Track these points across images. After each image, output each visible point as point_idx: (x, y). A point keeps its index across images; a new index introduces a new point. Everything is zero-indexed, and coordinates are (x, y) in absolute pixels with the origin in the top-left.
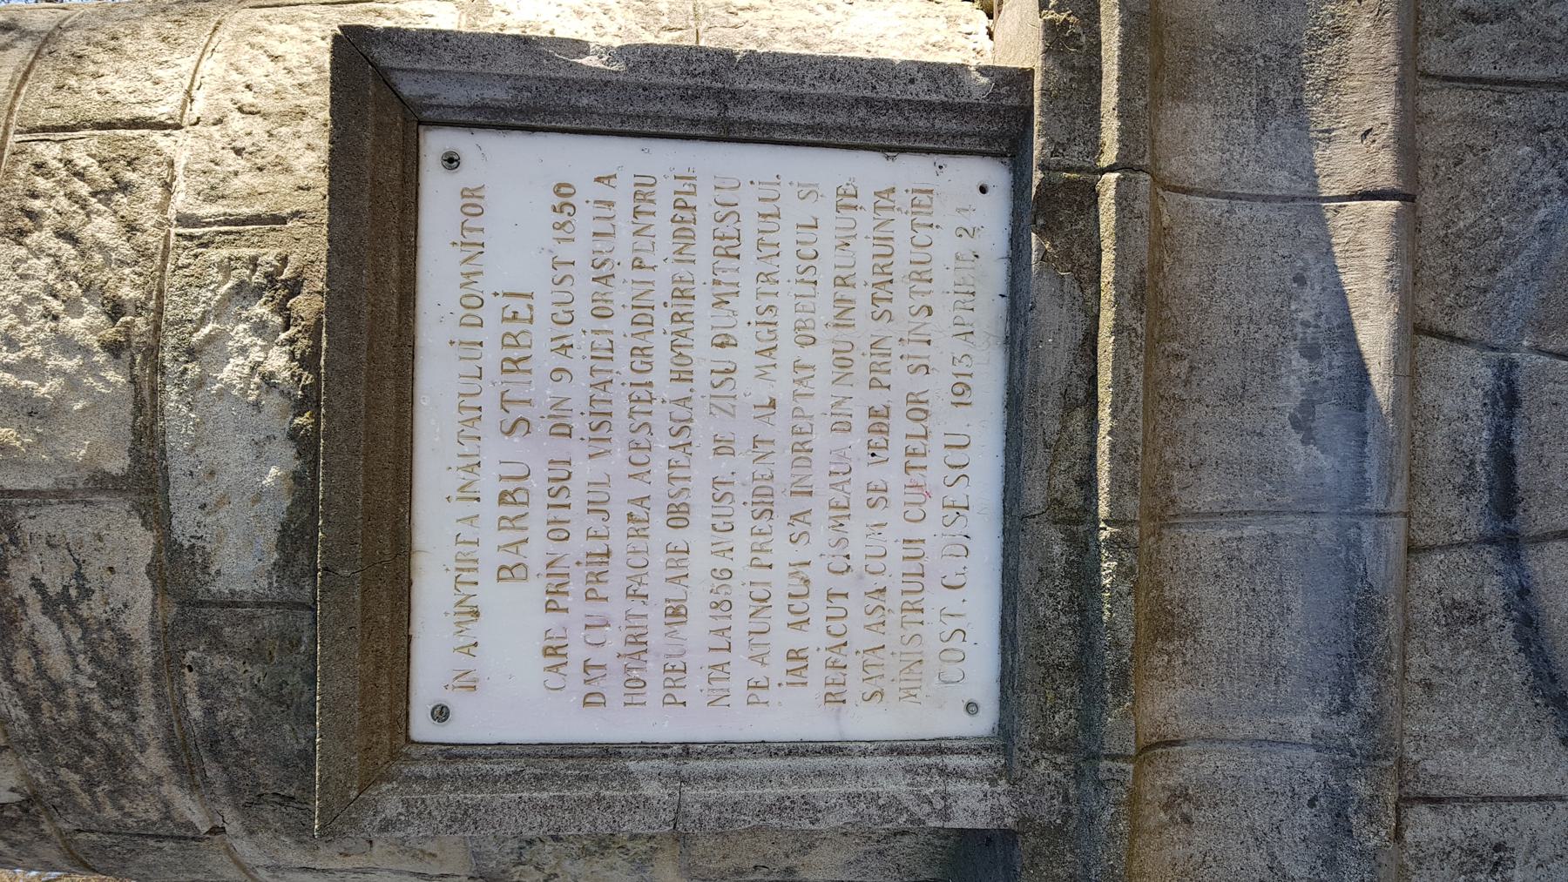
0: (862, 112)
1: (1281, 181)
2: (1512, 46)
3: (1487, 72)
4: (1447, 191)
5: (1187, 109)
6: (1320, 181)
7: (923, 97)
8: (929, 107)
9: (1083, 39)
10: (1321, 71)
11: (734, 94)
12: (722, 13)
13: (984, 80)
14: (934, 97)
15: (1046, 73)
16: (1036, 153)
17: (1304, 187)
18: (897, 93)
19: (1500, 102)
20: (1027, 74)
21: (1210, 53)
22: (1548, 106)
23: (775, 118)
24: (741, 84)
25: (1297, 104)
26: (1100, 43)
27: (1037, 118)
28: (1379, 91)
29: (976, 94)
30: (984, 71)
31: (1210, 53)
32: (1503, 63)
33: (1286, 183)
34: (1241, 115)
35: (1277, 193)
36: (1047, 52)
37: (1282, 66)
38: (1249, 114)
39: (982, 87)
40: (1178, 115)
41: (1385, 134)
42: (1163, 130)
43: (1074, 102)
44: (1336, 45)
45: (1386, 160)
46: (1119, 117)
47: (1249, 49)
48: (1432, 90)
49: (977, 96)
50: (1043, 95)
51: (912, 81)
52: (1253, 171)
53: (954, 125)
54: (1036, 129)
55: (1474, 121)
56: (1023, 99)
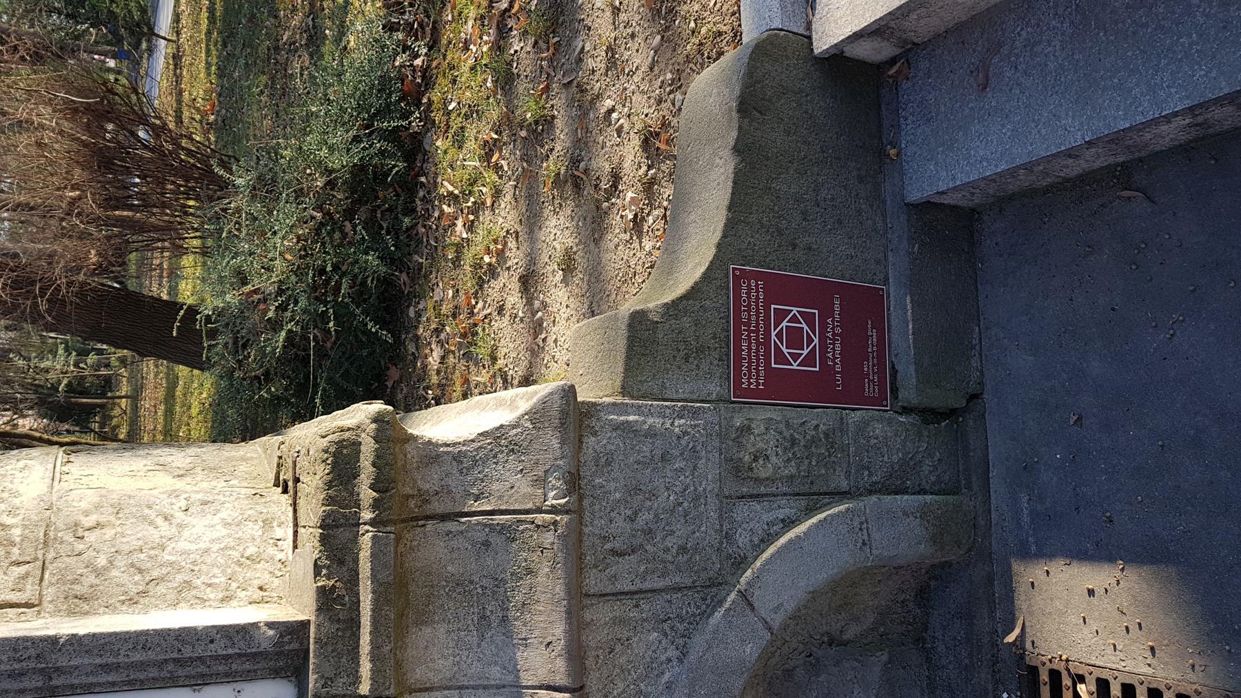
0: (171, 667)
1: (495, 674)
2: (643, 568)
3: (628, 587)
4: (605, 673)
5: (427, 630)
6: (521, 674)
7: (220, 652)
8: (227, 657)
9: (347, 598)
10: (520, 597)
11: (57, 669)
12: (69, 537)
13: (271, 632)
14: (230, 651)
15: (318, 626)
16: (311, 686)
17: (511, 678)
18: (199, 652)
19: (637, 606)
20: (305, 625)
21: (444, 587)
22: (667, 605)
23: (95, 680)
24: (63, 662)
25: (504, 619)
26: (359, 601)
27: (312, 660)
28: (555, 616)
29: (264, 645)
30: (270, 625)
31: (444, 587)
32: (637, 581)
33: (499, 675)
34: (467, 629)
35: (493, 683)
36: (319, 610)
37: (494, 593)
38: (472, 628)
39: (270, 638)
40: (420, 637)
41: (560, 646)
42: (409, 650)
43: (340, 646)
44: (528, 580)
45: (561, 664)
46: (371, 661)
47: (472, 582)
48: (592, 605)
49: (265, 645)
50: (316, 643)
51: (212, 642)
52: (476, 668)
53: (247, 666)
54: (311, 667)
55: (620, 621)
56: (301, 644)
